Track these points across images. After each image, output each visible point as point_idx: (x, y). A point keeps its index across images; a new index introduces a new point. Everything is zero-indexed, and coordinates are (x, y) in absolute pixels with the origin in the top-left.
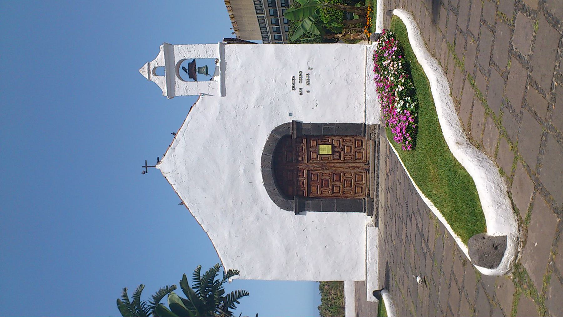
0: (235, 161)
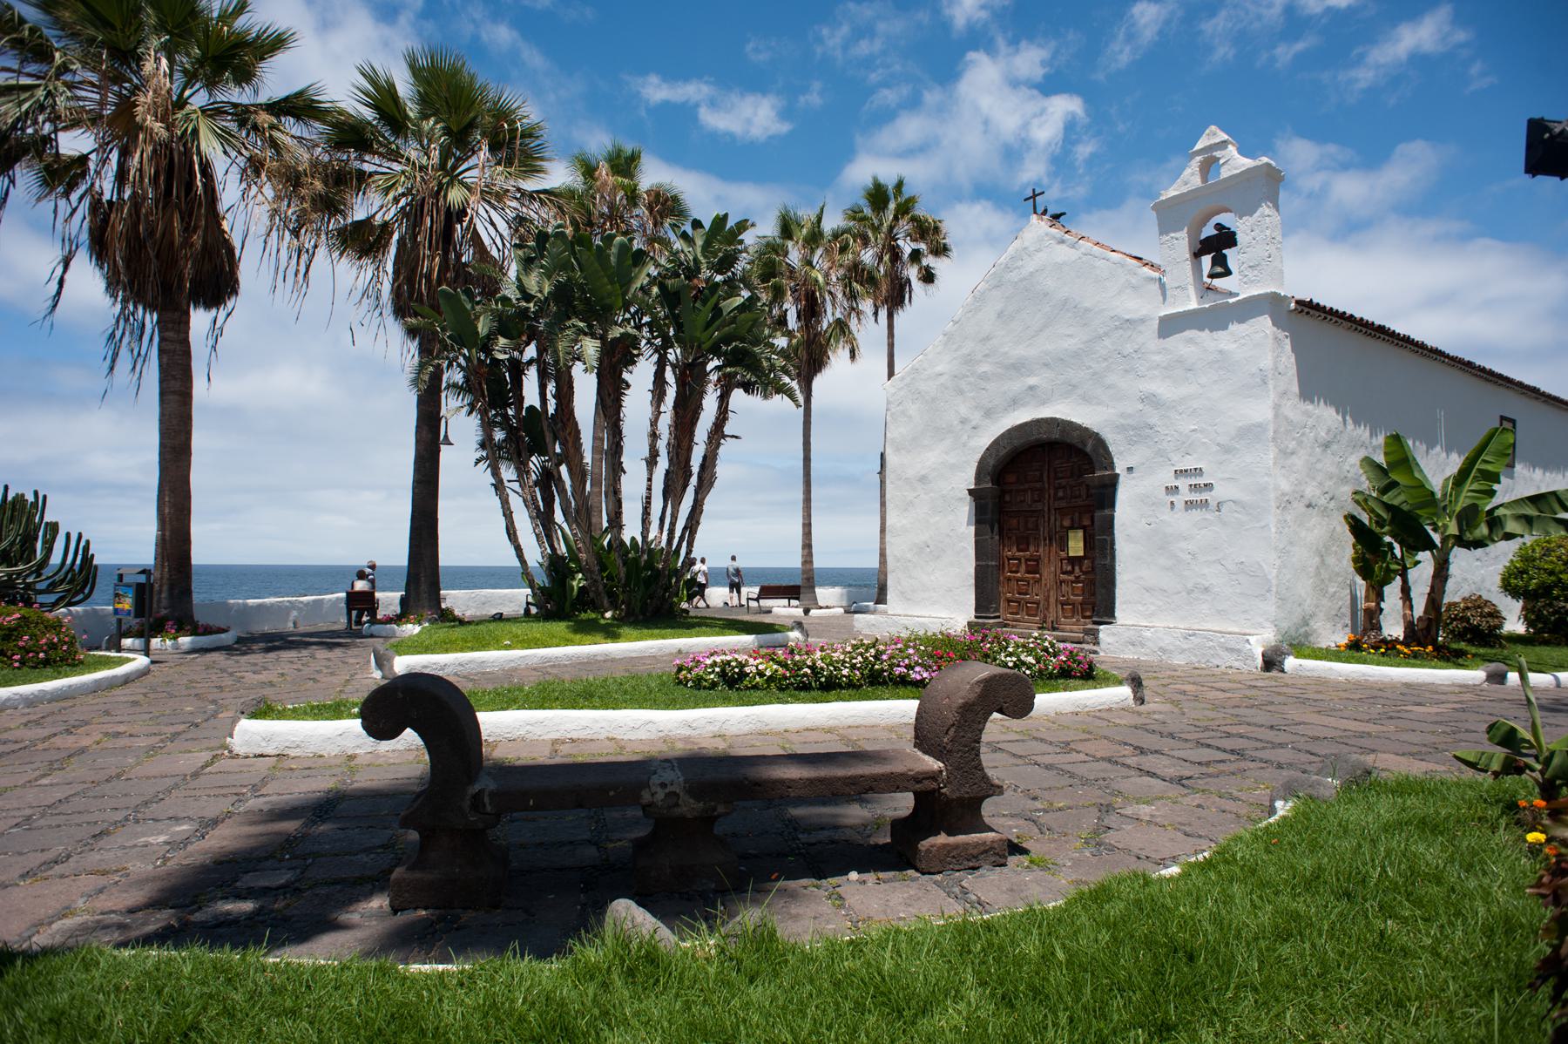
0: (1046, 365)
